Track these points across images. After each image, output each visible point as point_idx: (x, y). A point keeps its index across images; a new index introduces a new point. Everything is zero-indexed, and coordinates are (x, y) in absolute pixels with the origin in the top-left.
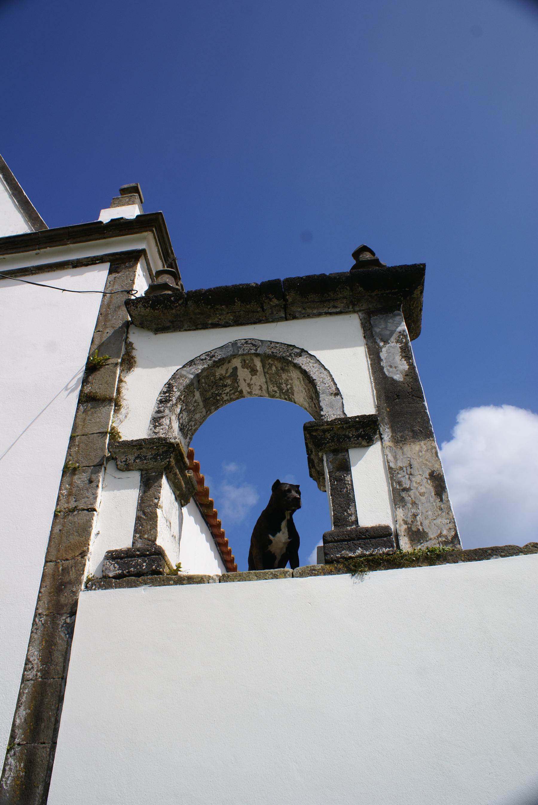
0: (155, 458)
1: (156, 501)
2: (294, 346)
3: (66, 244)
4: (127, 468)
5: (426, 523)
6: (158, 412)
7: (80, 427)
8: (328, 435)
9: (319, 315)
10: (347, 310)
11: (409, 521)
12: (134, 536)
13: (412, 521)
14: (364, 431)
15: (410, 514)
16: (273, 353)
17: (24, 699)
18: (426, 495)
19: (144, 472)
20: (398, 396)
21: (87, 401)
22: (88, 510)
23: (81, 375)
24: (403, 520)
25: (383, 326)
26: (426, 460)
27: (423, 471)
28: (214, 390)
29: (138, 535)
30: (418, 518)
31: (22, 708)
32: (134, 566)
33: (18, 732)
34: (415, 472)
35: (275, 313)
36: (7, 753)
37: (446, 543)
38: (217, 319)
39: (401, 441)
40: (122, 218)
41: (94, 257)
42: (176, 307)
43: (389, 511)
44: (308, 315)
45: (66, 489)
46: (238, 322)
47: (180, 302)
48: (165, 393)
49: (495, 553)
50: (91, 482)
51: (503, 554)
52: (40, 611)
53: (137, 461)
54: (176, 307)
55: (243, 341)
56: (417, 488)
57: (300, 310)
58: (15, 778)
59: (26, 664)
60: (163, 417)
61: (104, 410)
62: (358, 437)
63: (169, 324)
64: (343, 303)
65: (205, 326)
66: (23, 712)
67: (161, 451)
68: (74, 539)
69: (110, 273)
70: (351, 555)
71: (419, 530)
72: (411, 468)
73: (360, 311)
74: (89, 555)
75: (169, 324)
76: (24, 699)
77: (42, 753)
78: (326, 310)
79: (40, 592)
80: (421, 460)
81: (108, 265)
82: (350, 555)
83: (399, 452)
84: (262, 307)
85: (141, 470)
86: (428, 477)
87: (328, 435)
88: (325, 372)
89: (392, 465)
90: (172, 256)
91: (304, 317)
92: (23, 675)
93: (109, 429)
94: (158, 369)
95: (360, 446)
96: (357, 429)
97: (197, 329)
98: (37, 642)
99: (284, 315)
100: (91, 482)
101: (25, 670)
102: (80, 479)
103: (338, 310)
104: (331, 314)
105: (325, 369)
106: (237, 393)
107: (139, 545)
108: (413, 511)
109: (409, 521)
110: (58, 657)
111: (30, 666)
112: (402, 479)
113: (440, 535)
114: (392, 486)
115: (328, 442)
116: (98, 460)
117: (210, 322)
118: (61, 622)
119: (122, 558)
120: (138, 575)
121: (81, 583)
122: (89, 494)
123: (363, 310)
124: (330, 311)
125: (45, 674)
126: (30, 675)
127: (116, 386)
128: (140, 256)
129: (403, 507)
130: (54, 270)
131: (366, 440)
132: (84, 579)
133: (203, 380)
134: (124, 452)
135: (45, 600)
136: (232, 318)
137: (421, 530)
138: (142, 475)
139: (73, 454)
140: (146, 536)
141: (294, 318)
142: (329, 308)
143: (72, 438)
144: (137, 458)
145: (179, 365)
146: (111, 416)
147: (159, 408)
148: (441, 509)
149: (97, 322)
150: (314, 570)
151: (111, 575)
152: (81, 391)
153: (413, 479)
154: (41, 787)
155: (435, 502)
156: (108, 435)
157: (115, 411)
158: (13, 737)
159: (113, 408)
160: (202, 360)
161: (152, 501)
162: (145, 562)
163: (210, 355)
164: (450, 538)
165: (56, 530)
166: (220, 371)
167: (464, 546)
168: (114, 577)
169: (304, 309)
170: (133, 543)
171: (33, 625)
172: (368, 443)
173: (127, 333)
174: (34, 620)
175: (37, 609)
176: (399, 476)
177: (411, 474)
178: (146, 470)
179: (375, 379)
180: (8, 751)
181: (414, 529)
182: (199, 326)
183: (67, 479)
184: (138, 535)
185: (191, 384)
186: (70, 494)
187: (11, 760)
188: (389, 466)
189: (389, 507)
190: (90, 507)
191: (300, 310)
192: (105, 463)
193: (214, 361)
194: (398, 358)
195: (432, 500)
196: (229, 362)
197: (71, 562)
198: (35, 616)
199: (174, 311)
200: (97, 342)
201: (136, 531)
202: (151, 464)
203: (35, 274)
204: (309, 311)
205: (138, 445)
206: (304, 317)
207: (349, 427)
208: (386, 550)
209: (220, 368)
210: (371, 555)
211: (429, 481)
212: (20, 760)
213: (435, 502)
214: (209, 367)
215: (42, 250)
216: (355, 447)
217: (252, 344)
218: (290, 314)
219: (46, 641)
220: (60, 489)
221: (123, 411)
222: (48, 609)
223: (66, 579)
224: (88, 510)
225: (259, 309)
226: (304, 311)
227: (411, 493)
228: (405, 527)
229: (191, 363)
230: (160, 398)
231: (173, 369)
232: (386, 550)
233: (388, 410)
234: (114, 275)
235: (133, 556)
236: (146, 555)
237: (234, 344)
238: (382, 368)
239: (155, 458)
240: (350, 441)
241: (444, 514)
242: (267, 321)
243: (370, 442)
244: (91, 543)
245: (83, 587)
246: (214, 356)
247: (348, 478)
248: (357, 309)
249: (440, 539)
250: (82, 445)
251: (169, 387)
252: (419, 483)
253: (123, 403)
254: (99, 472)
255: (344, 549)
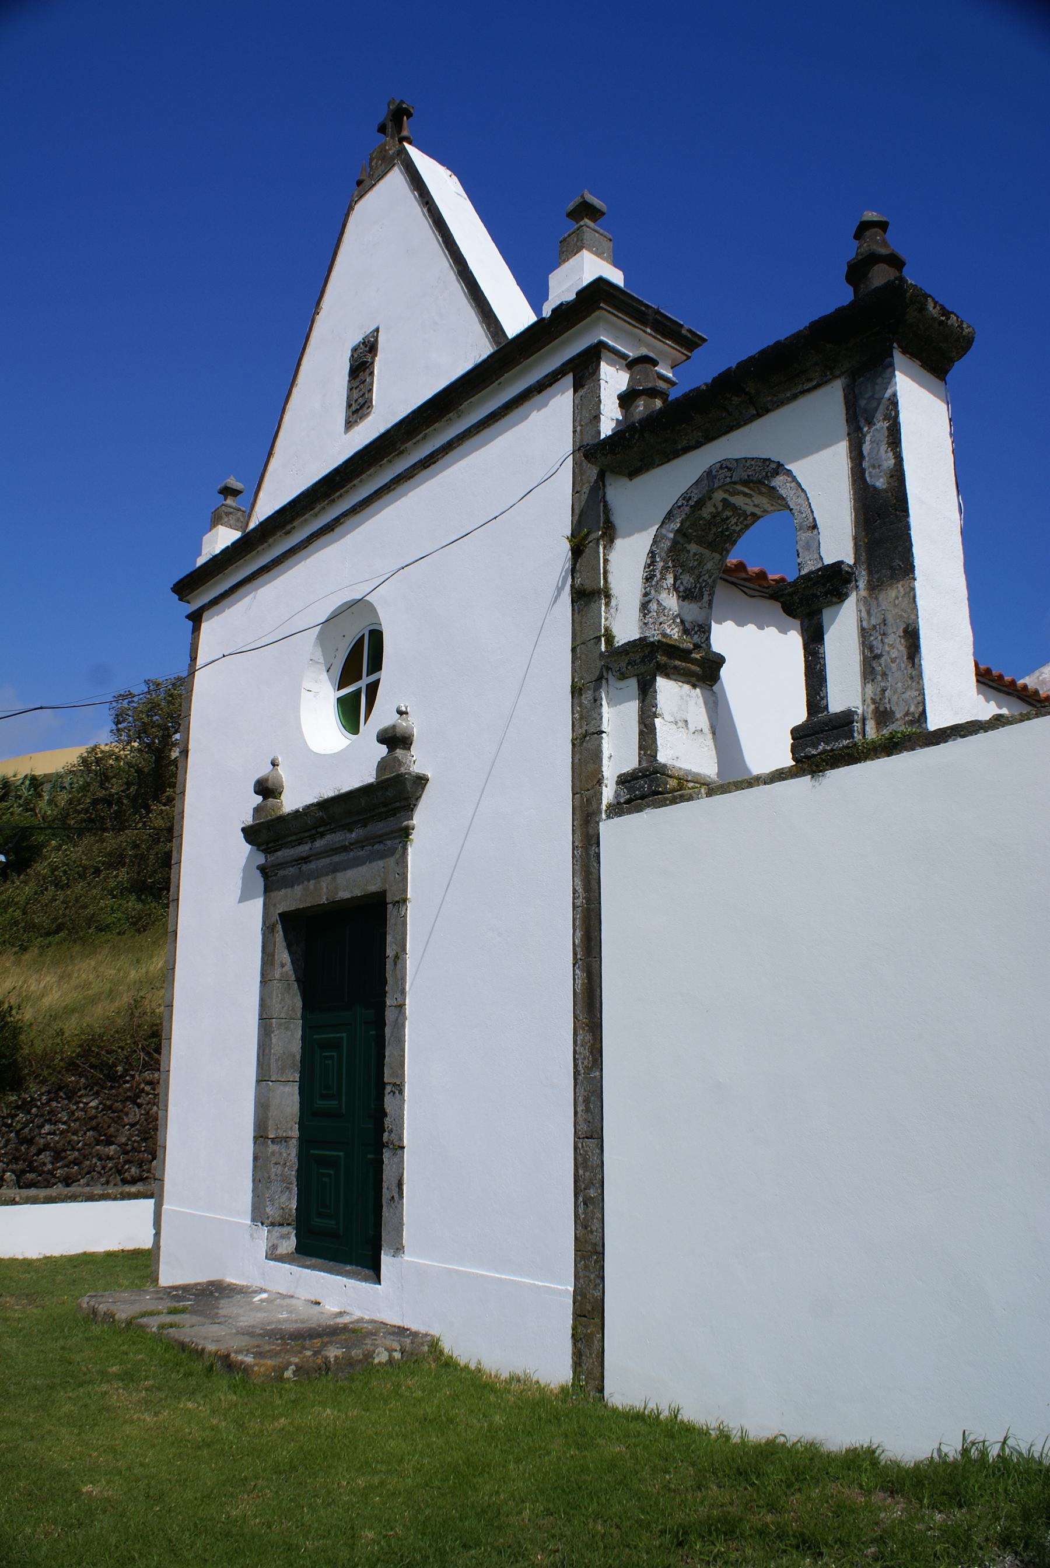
0: (643, 661)
1: (654, 709)
2: (769, 459)
3: (521, 363)
4: (623, 677)
5: (894, 698)
6: (646, 595)
7: (579, 634)
8: (796, 598)
9: (795, 397)
10: (825, 379)
11: (877, 698)
12: (640, 754)
13: (880, 699)
14: (831, 585)
15: (879, 689)
16: (748, 476)
17: (577, 923)
18: (898, 661)
19: (640, 677)
20: (879, 515)
21: (579, 598)
22: (596, 733)
23: (568, 565)
24: (872, 699)
25: (869, 394)
26: (902, 610)
27: (897, 627)
28: (715, 530)
29: (642, 752)
30: (887, 694)
31: (578, 930)
32: (639, 790)
33: (578, 949)
34: (890, 631)
35: (744, 411)
36: (574, 967)
37: (911, 723)
38: (685, 442)
39: (878, 586)
40: (562, 304)
41: (553, 372)
42: (635, 444)
43: (859, 689)
44: (782, 403)
45: (578, 712)
46: (710, 437)
47: (636, 437)
48: (649, 566)
49: (954, 733)
50: (595, 701)
51: (962, 733)
52: (576, 844)
53: (629, 668)
54: (635, 444)
55: (718, 465)
56: (889, 653)
57: (769, 398)
58: (583, 984)
59: (574, 893)
60: (650, 601)
61: (594, 606)
62: (826, 594)
63: (639, 464)
64: (816, 372)
65: (676, 454)
66: (579, 934)
67: (646, 652)
68: (591, 767)
69: (575, 392)
70: (814, 752)
71: (886, 708)
72: (885, 624)
73: (842, 374)
74: (605, 781)
75: (639, 464)
76: (577, 923)
77: (595, 965)
78: (800, 388)
79: (573, 826)
80: (896, 611)
81: (569, 379)
82: (813, 752)
83: (874, 603)
84: (727, 410)
85: (637, 676)
86: (902, 634)
87: (796, 598)
88: (803, 495)
89: (865, 624)
90: (650, 311)
91: (778, 406)
92: (574, 903)
93: (603, 631)
94: (636, 536)
95: (831, 604)
96: (824, 585)
97: (669, 460)
98: (579, 873)
99: (755, 412)
100: (595, 701)
101: (574, 899)
102: (587, 697)
103: (814, 383)
104: (809, 390)
105: (803, 490)
106: (749, 518)
107: (644, 764)
108: (883, 684)
109: (877, 698)
110: (594, 883)
111: (577, 895)
112: (874, 643)
113: (907, 714)
114: (863, 654)
115: (798, 608)
116: (598, 673)
117: (679, 447)
118: (592, 853)
119: (629, 782)
120: (642, 798)
121: (601, 813)
122: (595, 715)
123: (845, 372)
124: (806, 388)
125: (588, 900)
126: (578, 902)
127: (602, 571)
128: (600, 352)
129: (873, 680)
130: (522, 404)
131: (835, 596)
132: (604, 808)
133: (690, 531)
134: (615, 661)
135: (578, 833)
136: (700, 434)
137: (888, 709)
138: (638, 681)
139: (577, 669)
140: (649, 752)
141: (768, 411)
142: (803, 384)
143: (573, 650)
144: (628, 664)
145: (654, 525)
146: (603, 614)
147: (645, 588)
148: (912, 678)
149: (574, 477)
150: (783, 773)
151: (622, 801)
152: (572, 586)
153: (886, 641)
154: (598, 990)
155: (906, 669)
156: (603, 639)
157: (607, 604)
158: (575, 954)
159: (603, 601)
160: (679, 507)
161: (650, 710)
162: (646, 783)
163: (686, 497)
164: (917, 716)
165: (577, 761)
166: (706, 512)
167: (934, 723)
168: (625, 803)
169: (775, 395)
170: (640, 761)
171: (573, 858)
172: (839, 598)
173: (604, 486)
174: (573, 853)
175: (573, 842)
176: (872, 638)
177: (884, 634)
178: (642, 674)
179: (855, 493)
180: (574, 965)
181: (882, 709)
182: (671, 456)
183: (576, 701)
184: (642, 752)
185: (675, 542)
186: (581, 718)
187: (577, 971)
188: (862, 625)
189: (860, 683)
190: (598, 729)
191: (769, 398)
192: (605, 674)
193: (691, 506)
194: (883, 447)
195: (903, 666)
196: (710, 498)
197: (591, 792)
198: (573, 849)
199: (635, 449)
200: (577, 511)
201: (640, 748)
202: (643, 669)
203: (505, 415)
204: (782, 396)
205: (631, 646)
206: (778, 407)
207: (814, 584)
208: (845, 742)
209: (703, 509)
210: (832, 750)
211: (902, 640)
212: (582, 971)
213: (906, 669)
214: (688, 516)
215: (502, 378)
216: (828, 606)
217: (727, 467)
218: (761, 408)
219: (585, 872)
220: (573, 713)
221: (613, 603)
222: (582, 841)
223: (591, 811)
224: (596, 733)
225: (724, 415)
226: (775, 399)
227: (882, 661)
228: (872, 707)
229: (669, 516)
230: (646, 574)
231: (652, 531)
232: (845, 742)
233: (866, 540)
234: (581, 392)
235: (637, 778)
236: (646, 776)
237: (709, 474)
238: (863, 472)
239: (643, 661)
240: (819, 601)
241: (914, 684)
242: (739, 426)
243: (842, 597)
244: (604, 769)
245: (604, 816)
246: (690, 498)
247: (821, 651)
248: (838, 373)
249: (907, 718)
250: (583, 656)
251: (652, 554)
252: (892, 645)
253: (613, 592)
254: (600, 687)
255: (808, 746)
